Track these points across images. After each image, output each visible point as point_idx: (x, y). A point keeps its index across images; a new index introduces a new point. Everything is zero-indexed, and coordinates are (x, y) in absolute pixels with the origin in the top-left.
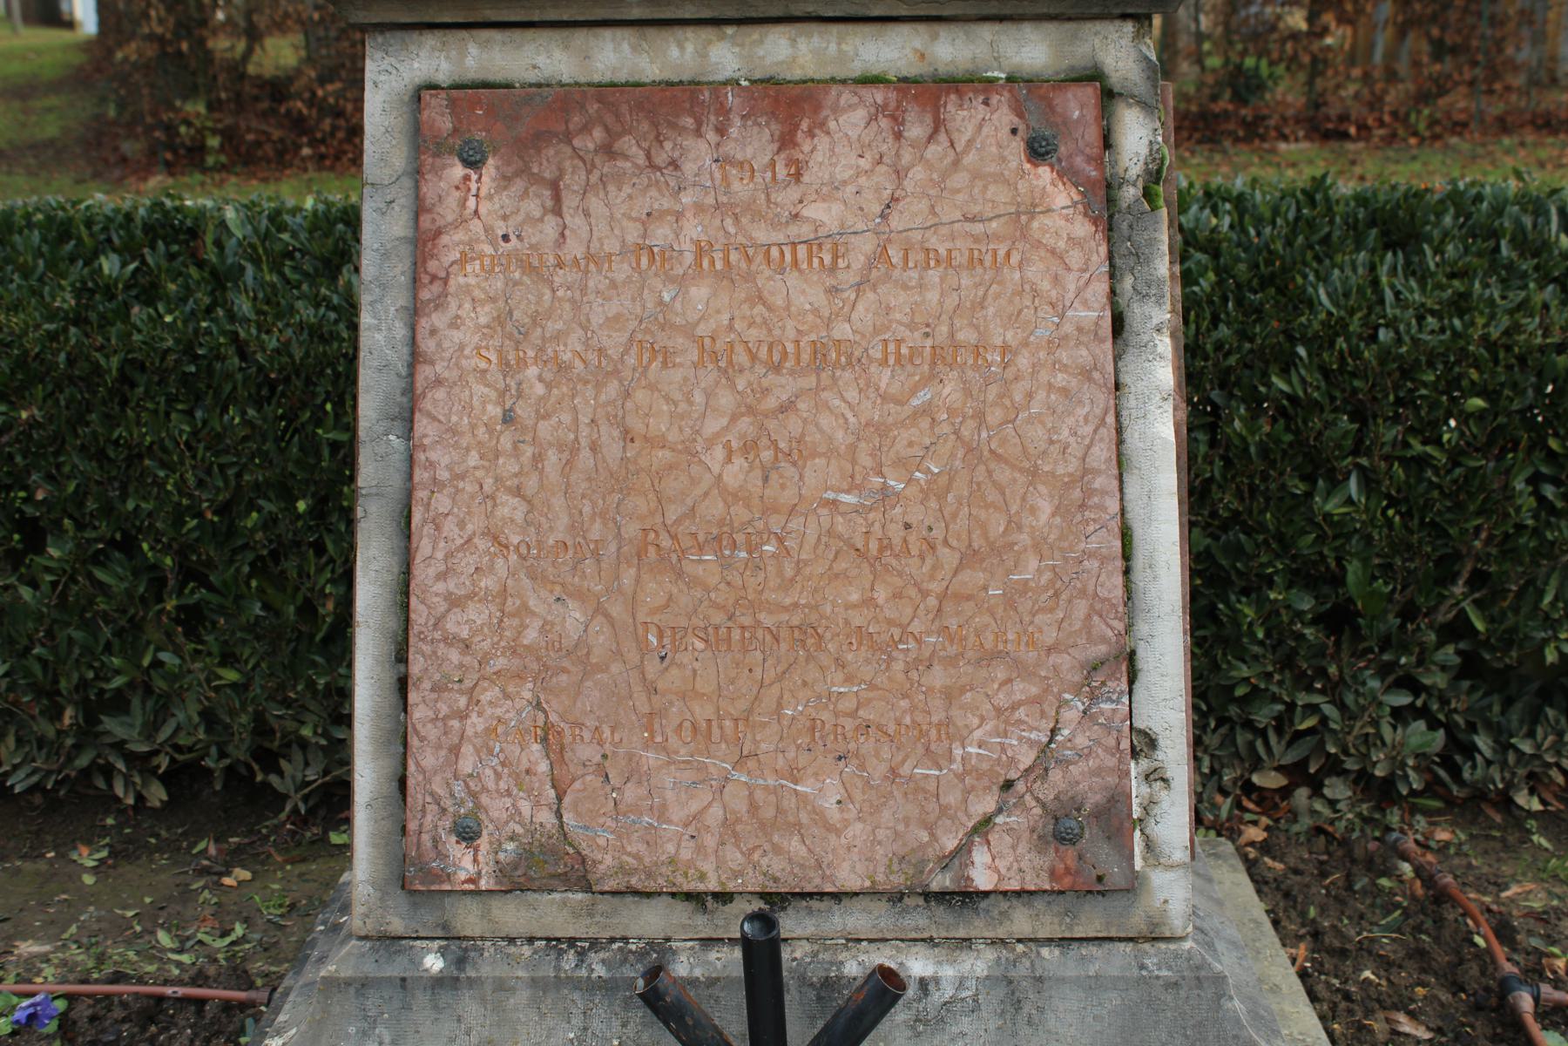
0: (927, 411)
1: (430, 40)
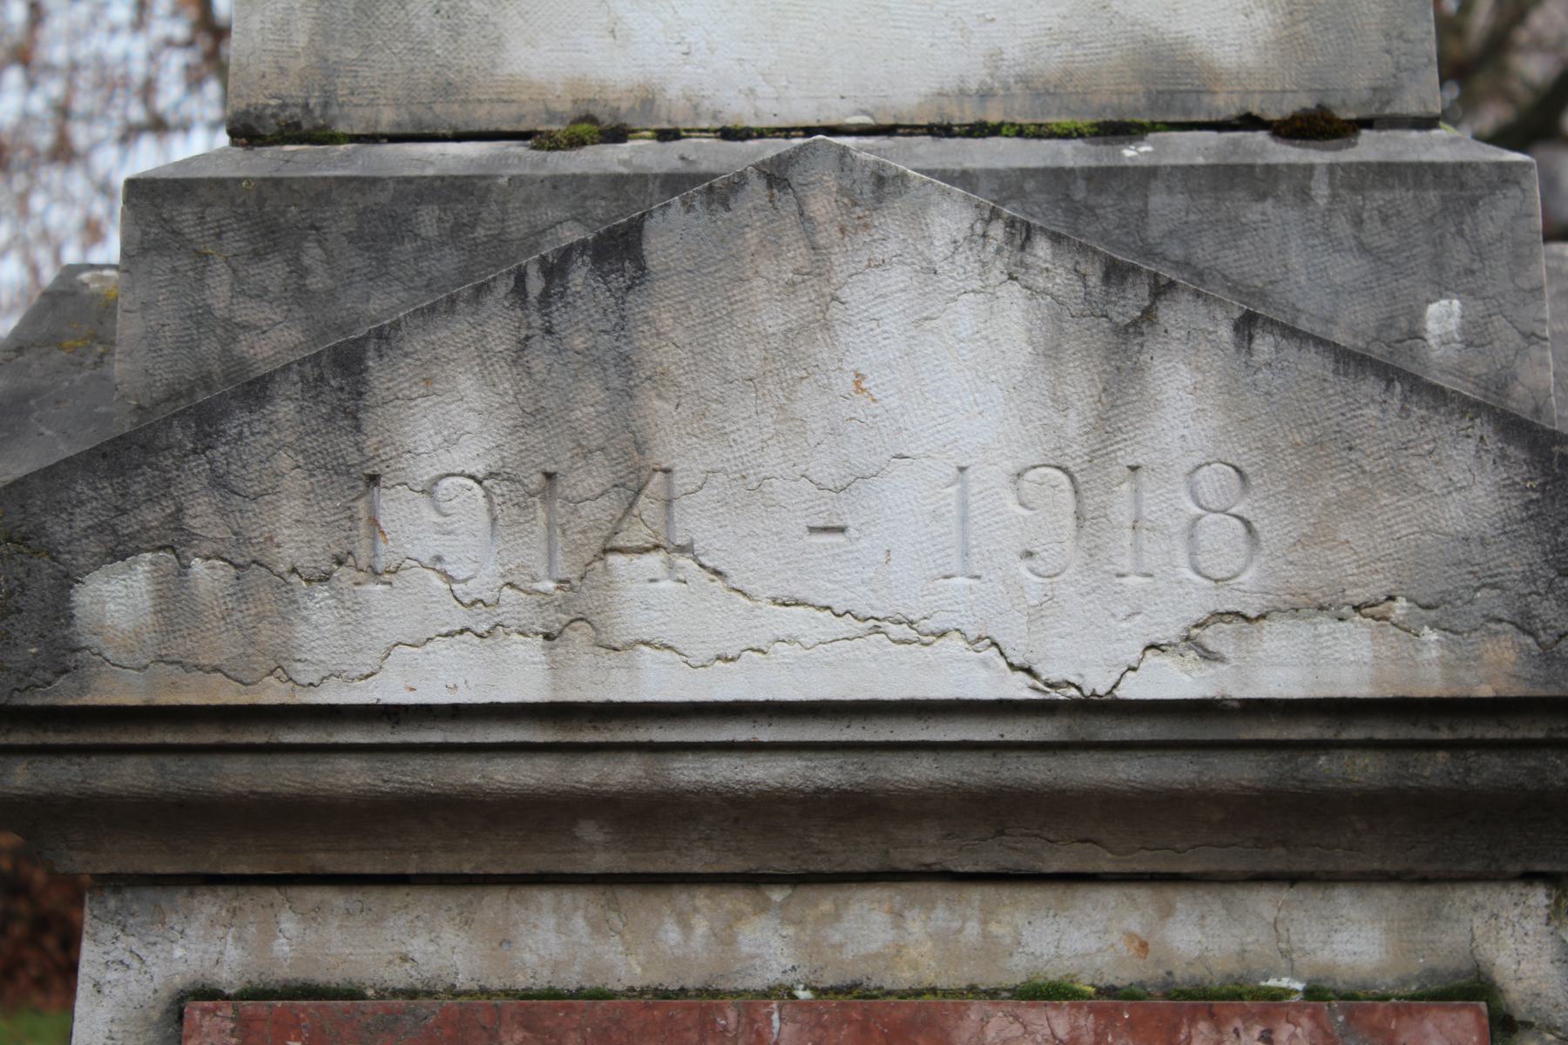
0: (1252, 244)
1: (209, 905)
